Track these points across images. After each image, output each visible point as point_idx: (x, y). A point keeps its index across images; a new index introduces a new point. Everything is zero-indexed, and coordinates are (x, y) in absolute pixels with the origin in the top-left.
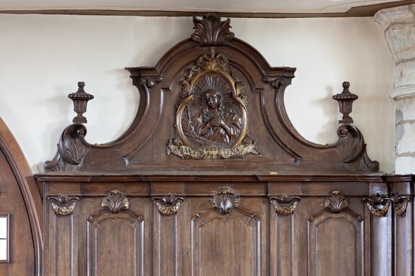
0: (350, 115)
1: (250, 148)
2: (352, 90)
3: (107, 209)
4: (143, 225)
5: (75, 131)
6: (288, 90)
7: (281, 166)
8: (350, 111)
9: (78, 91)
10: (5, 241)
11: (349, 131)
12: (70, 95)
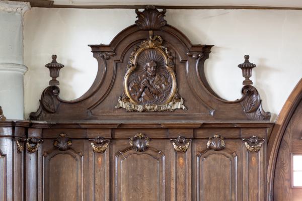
0: (57, 79)
1: (178, 105)
2: (251, 61)
3: (210, 148)
4: (236, 159)
5: (52, 91)
6: (208, 63)
7: (210, 116)
8: (58, 76)
9: (245, 62)
10: (294, 170)
11: (249, 90)
12: (47, 65)
